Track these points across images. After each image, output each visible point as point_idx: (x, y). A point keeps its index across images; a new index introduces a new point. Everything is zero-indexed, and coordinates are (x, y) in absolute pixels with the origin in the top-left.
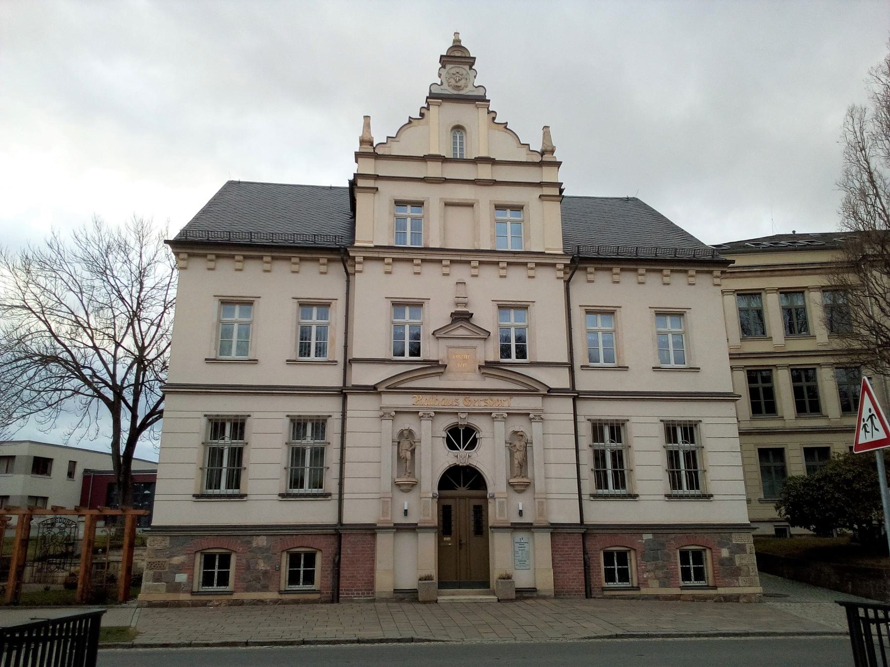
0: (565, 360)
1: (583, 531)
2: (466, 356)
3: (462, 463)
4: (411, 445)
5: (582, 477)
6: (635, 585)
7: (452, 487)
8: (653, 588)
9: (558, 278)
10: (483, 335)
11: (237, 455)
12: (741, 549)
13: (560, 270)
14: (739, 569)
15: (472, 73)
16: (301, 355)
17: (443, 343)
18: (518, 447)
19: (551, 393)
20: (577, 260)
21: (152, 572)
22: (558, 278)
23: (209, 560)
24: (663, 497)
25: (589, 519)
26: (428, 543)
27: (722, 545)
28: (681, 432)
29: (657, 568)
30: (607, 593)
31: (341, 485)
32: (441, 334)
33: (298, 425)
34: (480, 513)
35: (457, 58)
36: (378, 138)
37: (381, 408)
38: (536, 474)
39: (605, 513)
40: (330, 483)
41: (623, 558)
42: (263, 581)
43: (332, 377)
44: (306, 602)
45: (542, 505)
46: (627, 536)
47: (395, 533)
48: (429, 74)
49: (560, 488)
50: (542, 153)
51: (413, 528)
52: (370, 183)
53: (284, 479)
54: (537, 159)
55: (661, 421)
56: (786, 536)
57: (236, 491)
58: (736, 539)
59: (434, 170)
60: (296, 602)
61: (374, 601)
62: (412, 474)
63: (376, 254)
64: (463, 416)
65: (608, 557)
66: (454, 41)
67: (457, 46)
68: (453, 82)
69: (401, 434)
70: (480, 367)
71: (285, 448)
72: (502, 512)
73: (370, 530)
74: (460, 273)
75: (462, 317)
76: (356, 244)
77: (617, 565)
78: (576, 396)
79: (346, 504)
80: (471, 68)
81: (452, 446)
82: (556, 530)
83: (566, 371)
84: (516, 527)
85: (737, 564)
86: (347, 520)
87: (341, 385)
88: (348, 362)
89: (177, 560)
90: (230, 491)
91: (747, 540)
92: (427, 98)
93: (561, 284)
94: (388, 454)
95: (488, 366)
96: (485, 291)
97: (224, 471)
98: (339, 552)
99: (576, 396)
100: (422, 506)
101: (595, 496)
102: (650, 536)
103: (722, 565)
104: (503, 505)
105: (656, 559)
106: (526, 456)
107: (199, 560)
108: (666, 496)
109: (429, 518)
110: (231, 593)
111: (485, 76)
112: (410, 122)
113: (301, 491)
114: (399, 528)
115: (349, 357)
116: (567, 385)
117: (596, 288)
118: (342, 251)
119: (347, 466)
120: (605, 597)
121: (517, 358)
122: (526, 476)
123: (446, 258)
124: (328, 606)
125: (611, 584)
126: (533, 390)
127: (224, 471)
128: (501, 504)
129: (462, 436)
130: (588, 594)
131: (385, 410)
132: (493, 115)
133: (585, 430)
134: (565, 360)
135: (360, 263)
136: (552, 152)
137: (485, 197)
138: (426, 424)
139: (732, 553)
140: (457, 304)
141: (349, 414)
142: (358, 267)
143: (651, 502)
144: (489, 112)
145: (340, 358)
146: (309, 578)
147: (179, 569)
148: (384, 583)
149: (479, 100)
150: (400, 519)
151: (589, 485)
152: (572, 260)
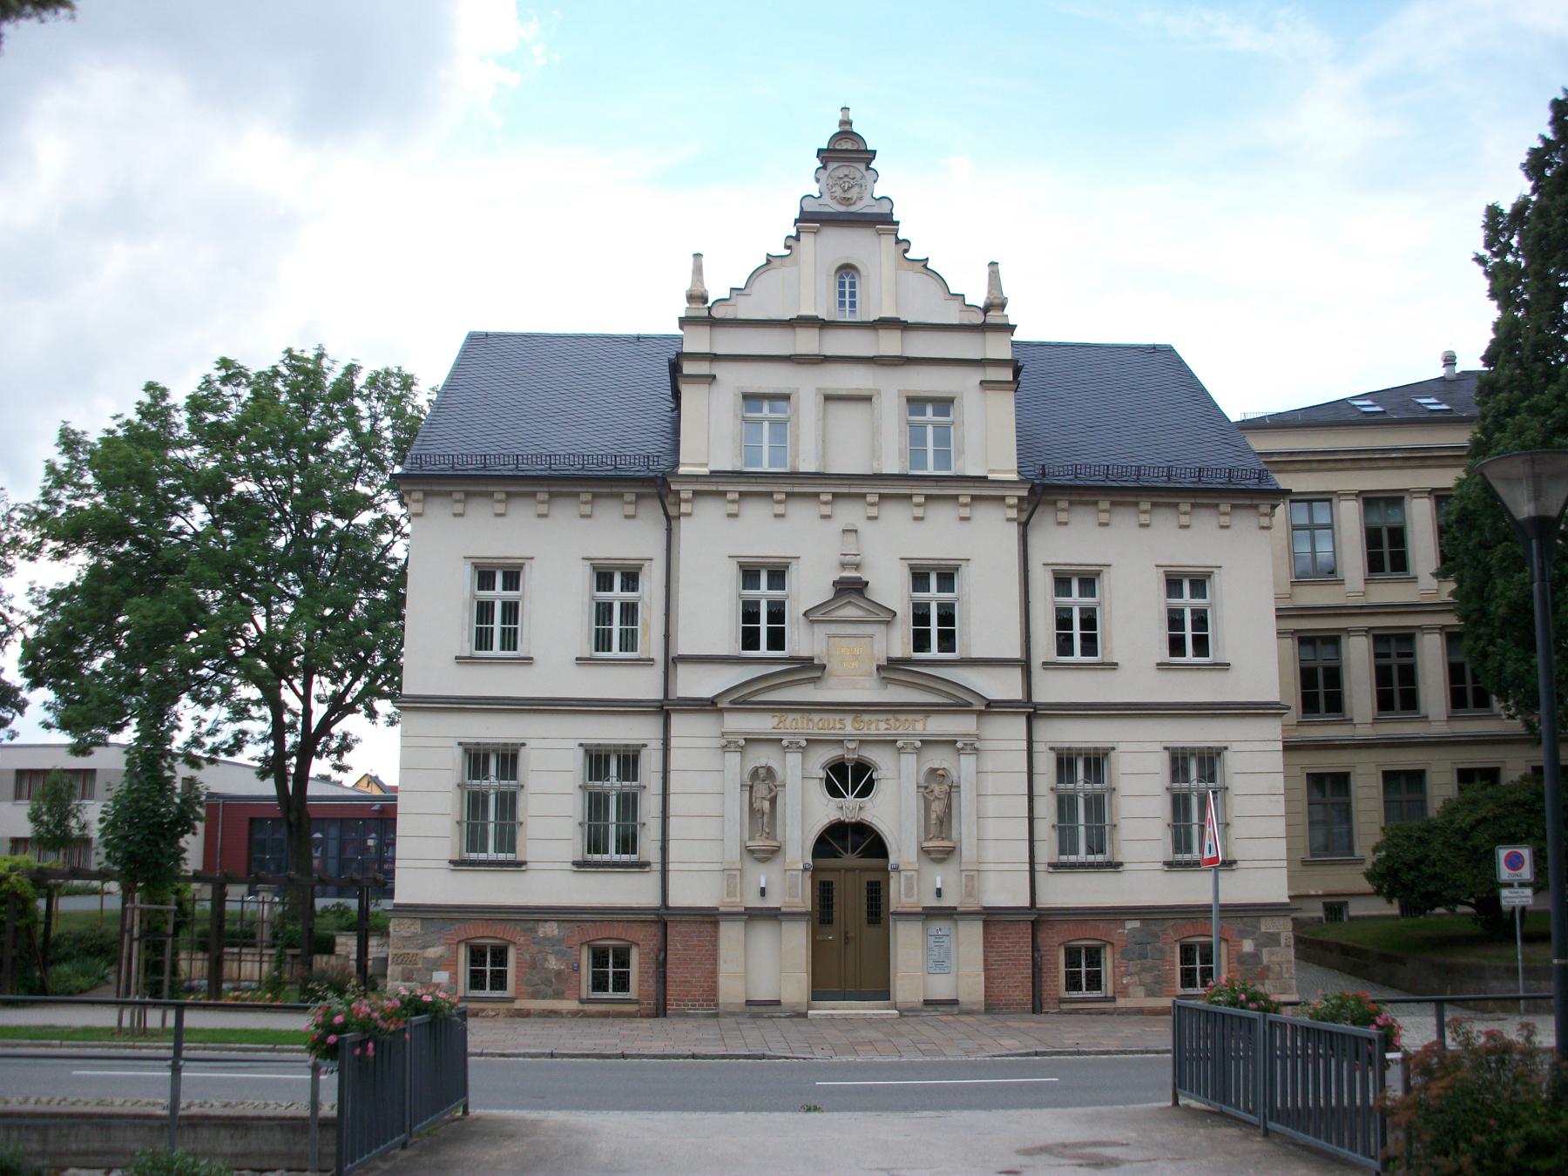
0: (1016, 652)
1: (1032, 918)
2: (857, 651)
3: (849, 817)
4: (771, 791)
5: (1036, 837)
6: (1110, 994)
7: (835, 855)
8: (1138, 999)
9: (1009, 520)
10: (884, 616)
11: (508, 803)
12: (1273, 939)
13: (1011, 507)
14: (1268, 968)
15: (869, 176)
16: (916, 650)
17: (821, 631)
18: (936, 793)
19: (993, 708)
20: (1039, 490)
21: (399, 968)
22: (1009, 520)
23: (477, 955)
24: (446, 864)
25: (1047, 899)
26: (797, 938)
27: (1244, 934)
28: (1195, 769)
29: (1144, 969)
30: (1065, 1006)
31: (664, 850)
32: (817, 616)
33: (597, 760)
34: (876, 896)
35: (846, 152)
36: (716, 290)
37: (723, 734)
38: (964, 836)
39: (1063, 892)
40: (648, 846)
41: (1094, 956)
42: (556, 985)
43: (646, 684)
44: (619, 1015)
45: (973, 877)
46: (1101, 925)
47: (746, 921)
48: (801, 181)
49: (1001, 857)
50: (987, 309)
51: (774, 915)
52: (702, 368)
53: (578, 838)
54: (978, 319)
55: (1166, 748)
56: (1341, 919)
57: (510, 856)
58: (1267, 926)
59: (806, 342)
60: (605, 1015)
61: (716, 1015)
62: (771, 835)
63: (716, 485)
64: (852, 746)
65: (1072, 956)
66: (843, 123)
67: (846, 132)
68: (839, 193)
69: (755, 774)
70: (879, 668)
71: (579, 793)
72: (909, 889)
73: (710, 918)
74: (849, 514)
75: (851, 588)
76: (682, 470)
77: (1085, 967)
78: (1032, 712)
79: (672, 877)
80: (868, 168)
81: (833, 791)
82: (992, 918)
83: (1016, 675)
84: (930, 914)
85: (1265, 961)
86: (674, 901)
87: (660, 696)
88: (672, 662)
89: (433, 952)
90: (502, 856)
91: (1283, 928)
92: (796, 221)
93: (1014, 529)
94: (735, 804)
95: (892, 668)
96: (890, 546)
97: (491, 827)
98: (664, 948)
99: (1032, 712)
100: (787, 882)
101: (1056, 867)
102: (1137, 924)
103: (1242, 963)
104: (913, 881)
105: (1143, 956)
106: (949, 806)
107: (463, 954)
108: (1166, 863)
109: (798, 900)
110: (511, 1000)
111: (892, 181)
112: (768, 262)
113: (606, 857)
114: (753, 916)
115: (672, 654)
116: (1017, 694)
117: (1070, 539)
118: (659, 482)
119: (673, 823)
120: (1062, 1012)
121: (503, 648)
122: (949, 838)
123: (826, 491)
124: (651, 1020)
125: (1075, 994)
126: (960, 703)
127: (491, 827)
128: (909, 879)
129: (850, 776)
130: (1037, 1007)
131: (731, 738)
132: (904, 246)
133: (1046, 765)
134: (1016, 652)
135: (686, 501)
136: (1002, 306)
137: (891, 387)
138: (794, 759)
139: (1258, 946)
140: (844, 566)
141: (673, 742)
142: (684, 508)
143: (1143, 877)
144: (898, 241)
145: (657, 653)
146: (622, 983)
147: (437, 964)
148: (730, 990)
149: (882, 221)
150: (754, 902)
151: (1047, 850)
152: (1031, 490)
